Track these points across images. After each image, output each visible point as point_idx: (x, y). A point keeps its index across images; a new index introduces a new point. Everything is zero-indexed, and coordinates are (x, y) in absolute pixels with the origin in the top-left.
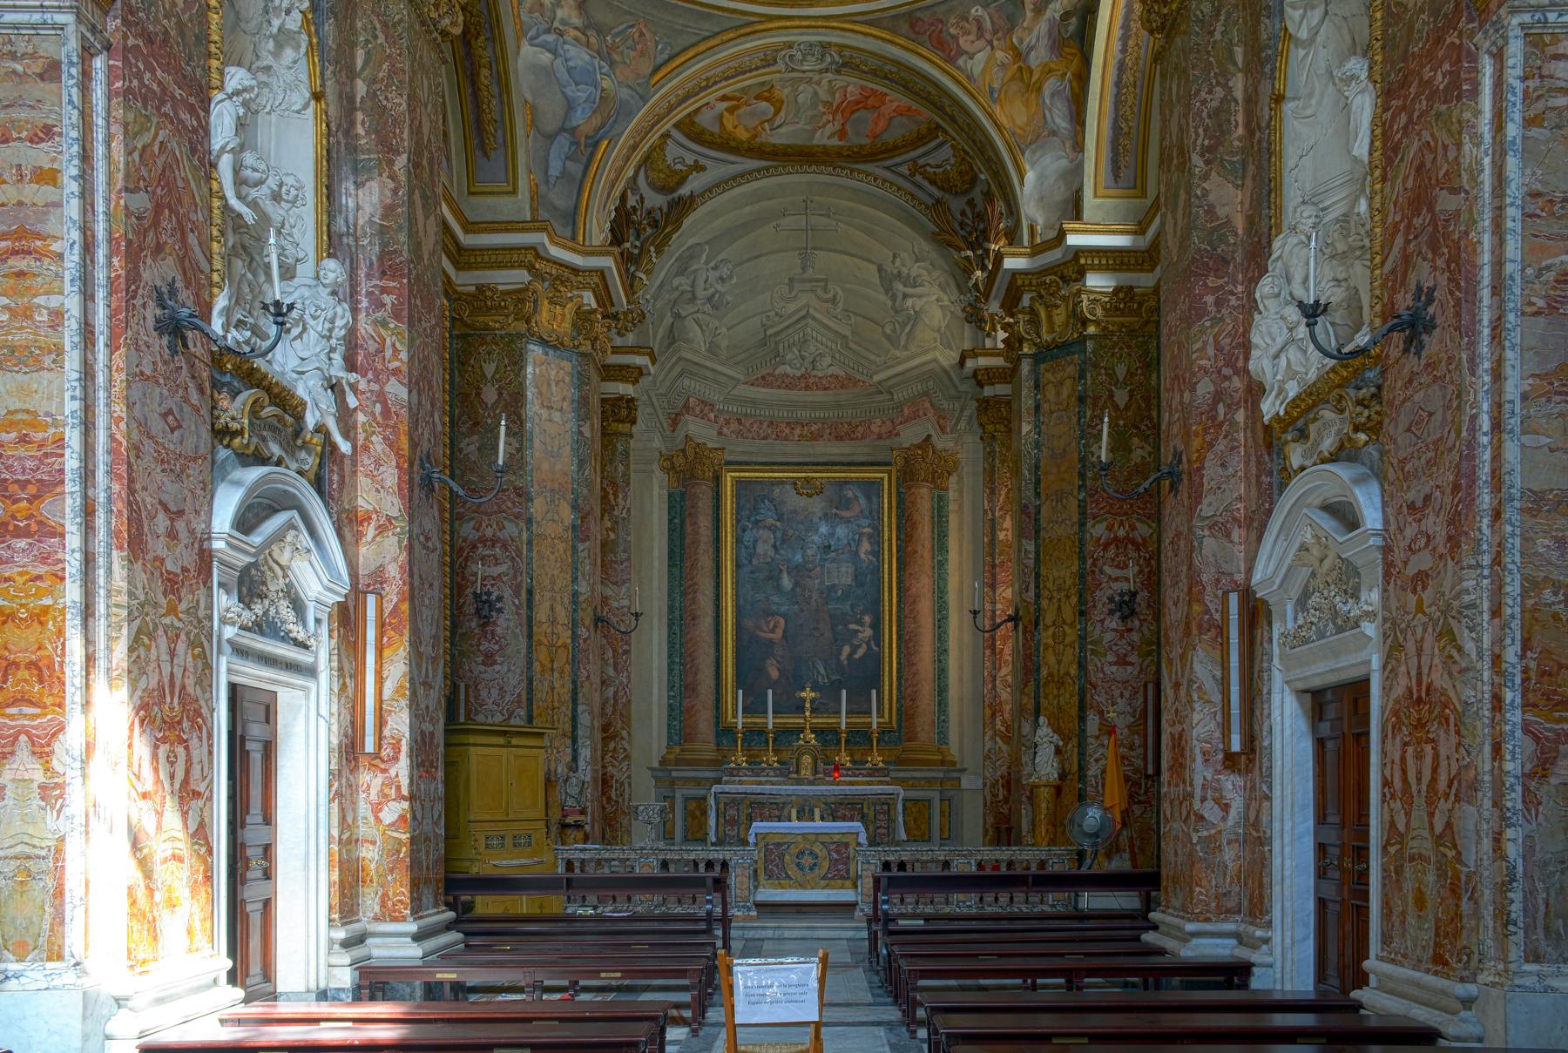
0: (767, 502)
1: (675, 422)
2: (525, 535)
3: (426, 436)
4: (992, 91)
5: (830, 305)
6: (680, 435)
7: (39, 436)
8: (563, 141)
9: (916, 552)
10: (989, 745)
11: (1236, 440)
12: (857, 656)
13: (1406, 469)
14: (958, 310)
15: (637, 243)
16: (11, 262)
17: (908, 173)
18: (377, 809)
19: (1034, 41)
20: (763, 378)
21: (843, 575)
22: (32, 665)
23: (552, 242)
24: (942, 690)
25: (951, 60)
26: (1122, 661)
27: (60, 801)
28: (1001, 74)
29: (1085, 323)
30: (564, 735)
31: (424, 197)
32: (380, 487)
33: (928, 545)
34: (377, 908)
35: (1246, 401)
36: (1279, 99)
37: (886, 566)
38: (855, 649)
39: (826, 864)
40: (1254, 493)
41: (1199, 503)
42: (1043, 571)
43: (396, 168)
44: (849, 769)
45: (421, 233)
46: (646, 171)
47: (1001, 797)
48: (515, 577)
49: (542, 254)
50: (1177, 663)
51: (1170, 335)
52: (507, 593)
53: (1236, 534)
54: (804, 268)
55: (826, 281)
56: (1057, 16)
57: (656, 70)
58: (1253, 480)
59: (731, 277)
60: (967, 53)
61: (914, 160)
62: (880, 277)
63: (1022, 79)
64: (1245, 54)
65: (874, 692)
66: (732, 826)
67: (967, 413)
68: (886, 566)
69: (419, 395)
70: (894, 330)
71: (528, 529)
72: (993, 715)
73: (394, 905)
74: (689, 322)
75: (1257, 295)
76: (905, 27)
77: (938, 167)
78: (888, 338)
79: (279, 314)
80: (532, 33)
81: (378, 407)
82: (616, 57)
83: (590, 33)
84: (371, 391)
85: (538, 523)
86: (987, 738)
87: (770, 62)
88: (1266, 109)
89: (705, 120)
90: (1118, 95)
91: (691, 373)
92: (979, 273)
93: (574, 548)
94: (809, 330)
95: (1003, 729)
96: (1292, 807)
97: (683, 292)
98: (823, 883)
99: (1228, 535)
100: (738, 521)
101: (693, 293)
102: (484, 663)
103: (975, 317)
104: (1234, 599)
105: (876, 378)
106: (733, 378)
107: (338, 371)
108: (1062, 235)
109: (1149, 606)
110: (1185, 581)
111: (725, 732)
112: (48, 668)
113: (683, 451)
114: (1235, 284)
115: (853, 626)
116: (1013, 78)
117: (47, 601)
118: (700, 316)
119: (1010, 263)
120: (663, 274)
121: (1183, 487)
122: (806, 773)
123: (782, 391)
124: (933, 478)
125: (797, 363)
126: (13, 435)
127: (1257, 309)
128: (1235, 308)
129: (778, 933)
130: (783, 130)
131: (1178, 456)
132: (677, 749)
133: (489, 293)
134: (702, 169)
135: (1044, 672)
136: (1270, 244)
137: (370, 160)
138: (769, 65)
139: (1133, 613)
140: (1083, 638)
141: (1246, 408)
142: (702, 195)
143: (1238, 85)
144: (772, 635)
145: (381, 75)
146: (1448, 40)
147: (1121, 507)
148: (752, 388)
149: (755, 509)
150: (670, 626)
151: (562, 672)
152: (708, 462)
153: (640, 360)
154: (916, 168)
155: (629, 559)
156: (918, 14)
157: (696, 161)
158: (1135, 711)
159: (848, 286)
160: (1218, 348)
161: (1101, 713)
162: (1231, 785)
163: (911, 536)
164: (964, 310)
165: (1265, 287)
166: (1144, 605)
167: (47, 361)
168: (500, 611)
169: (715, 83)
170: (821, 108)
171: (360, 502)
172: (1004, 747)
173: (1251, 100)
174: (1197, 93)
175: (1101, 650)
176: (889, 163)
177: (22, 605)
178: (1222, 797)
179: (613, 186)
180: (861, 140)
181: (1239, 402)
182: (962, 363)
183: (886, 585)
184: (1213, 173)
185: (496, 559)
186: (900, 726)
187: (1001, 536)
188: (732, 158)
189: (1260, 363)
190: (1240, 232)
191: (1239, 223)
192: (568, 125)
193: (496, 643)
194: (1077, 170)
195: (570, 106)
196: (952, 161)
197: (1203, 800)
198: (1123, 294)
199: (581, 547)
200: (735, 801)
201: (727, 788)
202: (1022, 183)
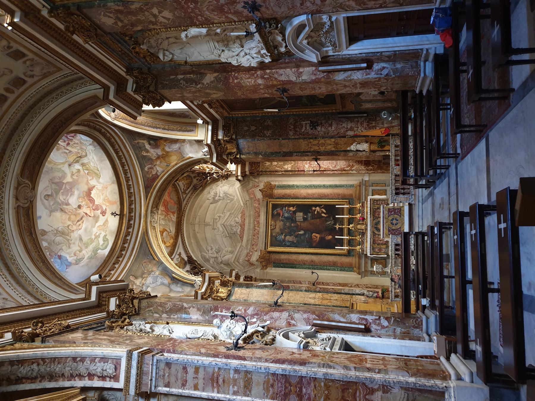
1: (252, 264)
4: (167, 166)
5: (221, 218)
6: (256, 263)
7: (271, 381)
12: (325, 212)
13: (291, 7)
14: (224, 182)
16: (220, 384)
17: (185, 195)
22: (343, 391)
24: (336, 186)
25: (158, 176)
26: (331, 125)
27: (388, 387)
28: (163, 163)
29: (232, 139)
30: (352, 297)
33: (291, 190)
34: (418, 330)
36: (186, 62)
38: (323, 212)
39: (396, 216)
41: (292, 81)
42: (302, 150)
43: (187, 307)
44: (362, 214)
47: (372, 168)
49: (203, 294)
50: (338, 87)
51: (243, 95)
54: (210, 225)
55: (214, 219)
56: (150, 146)
57: (154, 259)
58: (286, 65)
59: (211, 246)
61: (182, 193)
63: (165, 157)
65: (337, 206)
73: (417, 324)
74: (223, 259)
75: (237, 65)
78: (231, 201)
85: (283, 300)
91: (238, 259)
92: (214, 175)
93: (291, 290)
96: (385, 44)
97: (215, 261)
98: (402, 216)
99: (301, 72)
101: (215, 258)
103: (227, 176)
104: (321, 68)
105: (242, 205)
108: (207, 145)
111: (349, 253)
112: (344, 386)
113: (261, 262)
115: (316, 213)
116: (164, 160)
117: (322, 384)
118: (222, 256)
120: (209, 267)
121: (287, 87)
122: (363, 227)
123: (245, 232)
126: (271, 389)
130: (171, 229)
132: (355, 269)
135: (333, 149)
136: (223, 63)
139: (316, 122)
140: (323, 138)
143: (180, 77)
145: (161, 309)
146: (183, 4)
152: (265, 255)
154: (184, 192)
156: (146, 185)
160: (249, 78)
161: (347, 131)
162: (376, 67)
163: (289, 195)
164: (224, 180)
165: (234, 63)
167: (249, 376)
170: (166, 218)
172: (355, 167)
173: (184, 73)
175: (327, 131)
176: (182, 200)
177: (324, 392)
178: (381, 69)
180: (175, 208)
182: (239, 180)
186: (348, 199)
187: (289, 169)
188: (178, 245)
189: (254, 64)
192: (168, 285)
194: (190, 141)
196: (183, 182)
197: (381, 74)
199: (291, 288)
200: (373, 249)
201: (368, 251)
202: (192, 158)
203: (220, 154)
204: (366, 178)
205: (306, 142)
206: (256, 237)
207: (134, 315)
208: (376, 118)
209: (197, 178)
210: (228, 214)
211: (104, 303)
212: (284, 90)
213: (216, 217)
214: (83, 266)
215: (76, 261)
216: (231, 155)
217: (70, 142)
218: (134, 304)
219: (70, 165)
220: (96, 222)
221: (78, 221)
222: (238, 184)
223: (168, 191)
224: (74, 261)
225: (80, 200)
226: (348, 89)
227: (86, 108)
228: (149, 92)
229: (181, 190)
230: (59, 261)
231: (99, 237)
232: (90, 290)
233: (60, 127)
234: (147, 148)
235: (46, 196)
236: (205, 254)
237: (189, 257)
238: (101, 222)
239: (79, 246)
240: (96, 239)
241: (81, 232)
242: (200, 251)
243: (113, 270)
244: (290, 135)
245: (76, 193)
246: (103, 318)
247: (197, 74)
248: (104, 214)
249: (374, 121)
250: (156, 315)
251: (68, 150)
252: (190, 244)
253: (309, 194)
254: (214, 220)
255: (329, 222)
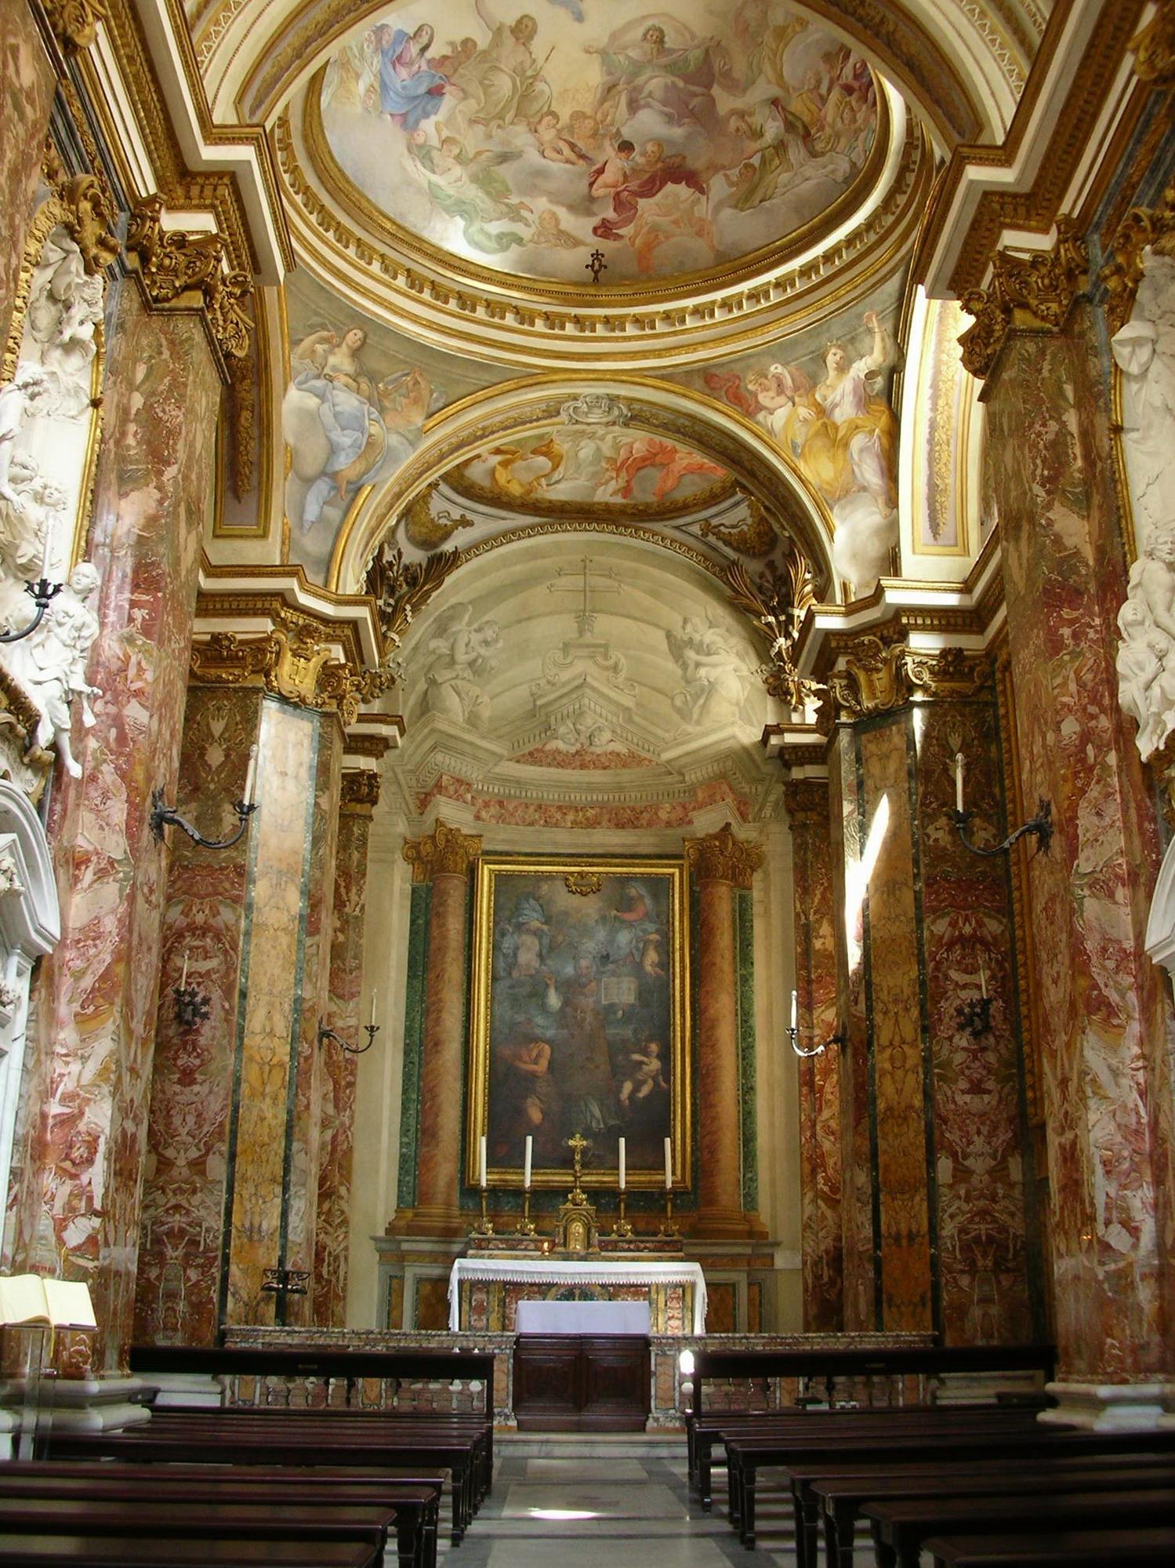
0: (532, 902)
1: (424, 801)
2: (243, 924)
3: (162, 770)
4: (794, 446)
8: (322, 487)
9: (714, 964)
10: (809, 1210)
11: (1109, 785)
14: (758, 680)
15: (392, 601)
18: (60, 1226)
19: (838, 398)
20: (531, 754)
21: (623, 992)
23: (302, 588)
24: (748, 1138)
26: (976, 1088)
28: (804, 430)
29: (911, 688)
30: (273, 1180)
31: (189, 512)
32: (104, 824)
33: (728, 955)
35: (1117, 742)
36: (1118, 429)
37: (677, 981)
40: (1137, 841)
43: (164, 479)
44: (630, 1242)
45: (182, 548)
46: (407, 525)
47: (826, 1279)
48: (227, 974)
49: (289, 599)
52: (216, 995)
53: (1121, 893)
54: (581, 632)
55: (606, 646)
57: (430, 416)
58: (1135, 830)
59: (496, 641)
60: (766, 408)
61: (706, 520)
62: (669, 643)
63: (827, 435)
64: (1075, 391)
66: (480, 1314)
67: (772, 798)
68: (677, 981)
69: (160, 722)
70: (686, 702)
71: (247, 917)
72: (814, 1172)
75: (1120, 623)
76: (699, 382)
77: (733, 527)
78: (679, 711)
79: (43, 594)
80: (301, 378)
81: (113, 732)
82: (387, 403)
83: (361, 380)
84: (107, 714)
86: (806, 1201)
87: (552, 412)
88: (1106, 440)
89: (476, 473)
90: (931, 452)
92: (781, 641)
93: (300, 942)
94: (586, 701)
95: (826, 1189)
97: (440, 656)
99: (1111, 895)
100: (496, 923)
101: (452, 656)
102: (180, 1082)
103: (778, 690)
106: (493, 753)
107: (78, 683)
108: (880, 591)
109: (1005, 1019)
110: (1066, 951)
111: (470, 1191)
113: (433, 837)
114: (1092, 615)
115: (637, 1057)
116: (817, 434)
118: (459, 682)
119: (822, 623)
120: (418, 636)
121: (1056, 842)
122: (578, 1247)
123: (552, 770)
124: (734, 873)
125: (572, 737)
127: (1122, 638)
128: (1094, 642)
129: (545, 1449)
130: (559, 486)
131: (1045, 807)
132: (409, 1214)
133: (226, 643)
134: (470, 524)
135: (881, 1105)
136: (1126, 572)
137: (138, 470)
138: (551, 417)
139: (987, 1028)
140: (927, 1061)
141: (1118, 750)
142: (468, 551)
143: (1072, 420)
144: (535, 1067)
145: (162, 387)
147: (966, 899)
148: (517, 766)
149: (517, 909)
150: (407, 1054)
151: (275, 1099)
153: (385, 730)
154: (708, 528)
155: (359, 967)
156: (713, 370)
157: (463, 516)
158: (996, 1151)
159: (632, 652)
160: (1081, 685)
161: (954, 1155)
164: (765, 681)
166: (999, 1018)
168: (205, 1016)
169: (493, 433)
170: (604, 464)
171: (80, 841)
172: (829, 1213)
173: (1087, 434)
174: (1031, 425)
176: (680, 521)
178: (1130, 1219)
179: (372, 534)
180: (645, 495)
181: (1108, 745)
182: (765, 740)
183: (678, 1004)
184: (1056, 504)
185: (206, 952)
186: (694, 1186)
187: (818, 944)
189: (1129, 692)
190: (1091, 563)
191: (1089, 553)
192: (329, 470)
193: (199, 1055)
195: (333, 450)
197: (1108, 1223)
198: (951, 663)
199: (309, 941)
203: (850, 644)
204: (784, 1260)
205: (907, 991)
206: (532, 814)
207: (142, 293)
208: (1008, 1270)
209: (768, 574)
210: (629, 702)
211: (195, 191)
212: (1043, 832)
213: (615, 655)
214: (404, 169)
215: (420, 147)
216: (848, 687)
217: (855, 96)
218: (187, 294)
219: (775, 102)
220: (572, 208)
221: (572, 146)
222: (750, 735)
223: (707, 462)
224: (420, 140)
225: (650, 148)
226: (1056, 1095)
227: (937, 102)
228: (1007, 311)
229: (716, 515)
230: (422, 90)
231: (512, 219)
232: (240, 139)
233: (860, 20)
234: (855, 365)
235: (657, 34)
236: (466, 618)
237: (452, 561)
238: (569, 221)
239: (479, 153)
240: (506, 210)
241: (533, 156)
242: (480, 597)
243: (386, 270)
244: (933, 922)
245: (677, 132)
246: (129, 185)
247: (1084, 482)
248: (600, 232)
249: (996, 1263)
250: (141, 371)
251: (829, 90)
252: (505, 562)
253: (712, 1027)
254: (600, 646)
255: (597, 1113)
